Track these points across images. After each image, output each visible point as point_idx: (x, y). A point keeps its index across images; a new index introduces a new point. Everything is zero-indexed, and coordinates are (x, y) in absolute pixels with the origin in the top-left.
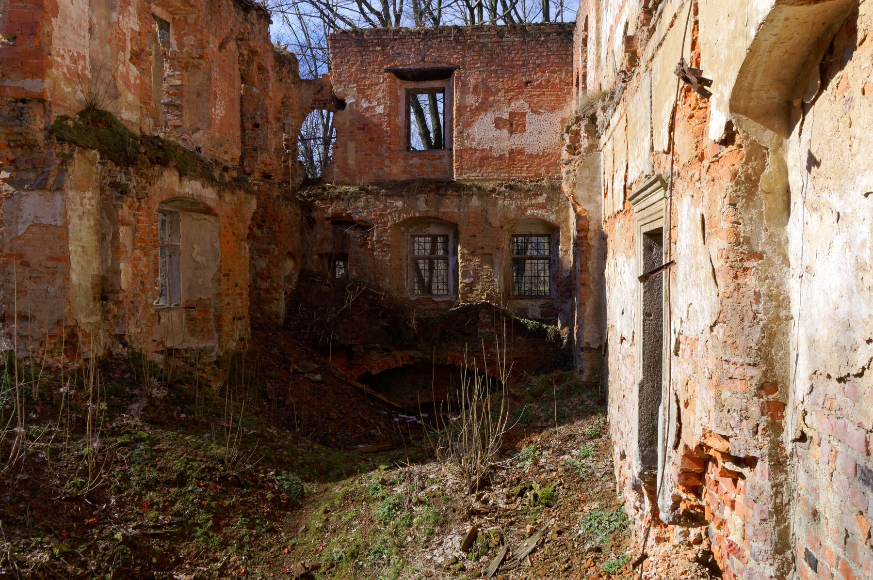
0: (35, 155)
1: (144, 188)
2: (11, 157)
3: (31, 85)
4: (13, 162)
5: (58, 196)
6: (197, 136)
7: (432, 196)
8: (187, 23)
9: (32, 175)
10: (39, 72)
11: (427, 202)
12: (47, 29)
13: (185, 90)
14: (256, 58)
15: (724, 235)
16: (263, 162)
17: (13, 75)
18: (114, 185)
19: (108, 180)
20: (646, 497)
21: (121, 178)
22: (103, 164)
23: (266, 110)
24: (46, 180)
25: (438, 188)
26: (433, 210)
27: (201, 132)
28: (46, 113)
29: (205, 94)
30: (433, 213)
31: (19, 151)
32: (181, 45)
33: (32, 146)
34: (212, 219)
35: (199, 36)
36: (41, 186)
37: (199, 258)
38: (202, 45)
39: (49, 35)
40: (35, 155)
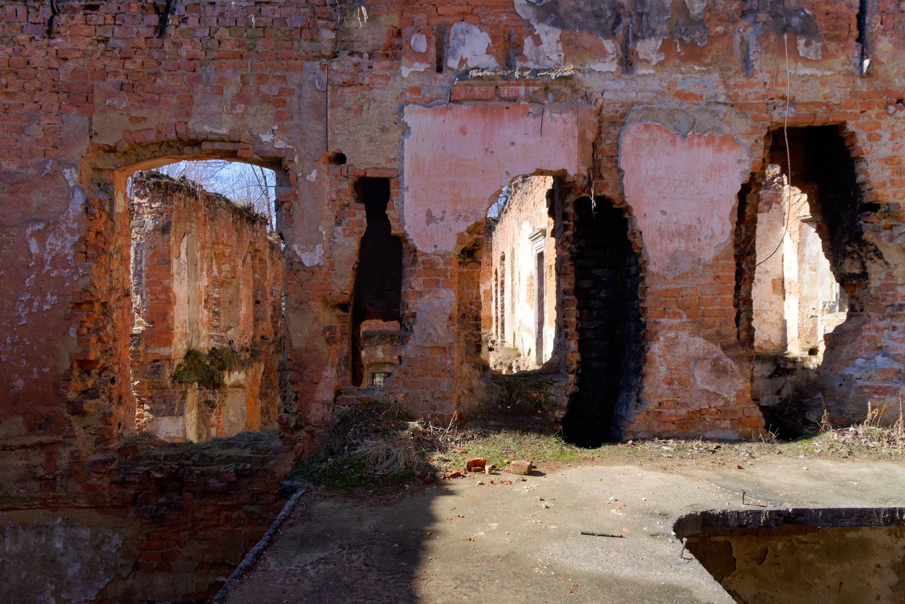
0: (165, 394)
1: (223, 401)
2: (150, 395)
3: (164, 351)
4: (151, 398)
5: (181, 419)
6: (230, 332)
7: (387, 346)
8: (224, 255)
9: (164, 407)
10: (168, 343)
11: (384, 351)
12: (172, 314)
13: (222, 300)
14: (258, 254)
15: (652, 260)
16: (263, 329)
17: (152, 346)
18: (208, 403)
19: (203, 399)
20: (812, 484)
21: (211, 397)
22: (200, 389)
23: (265, 291)
24: (173, 409)
25: (392, 341)
26: (388, 357)
27: (233, 330)
28: (171, 365)
29: (234, 302)
30: (388, 360)
31: (155, 391)
32: (220, 272)
33: (163, 389)
34: (241, 390)
35: (232, 263)
36: (171, 413)
37: (232, 419)
38: (234, 270)
39: (173, 318)
40: (165, 394)
